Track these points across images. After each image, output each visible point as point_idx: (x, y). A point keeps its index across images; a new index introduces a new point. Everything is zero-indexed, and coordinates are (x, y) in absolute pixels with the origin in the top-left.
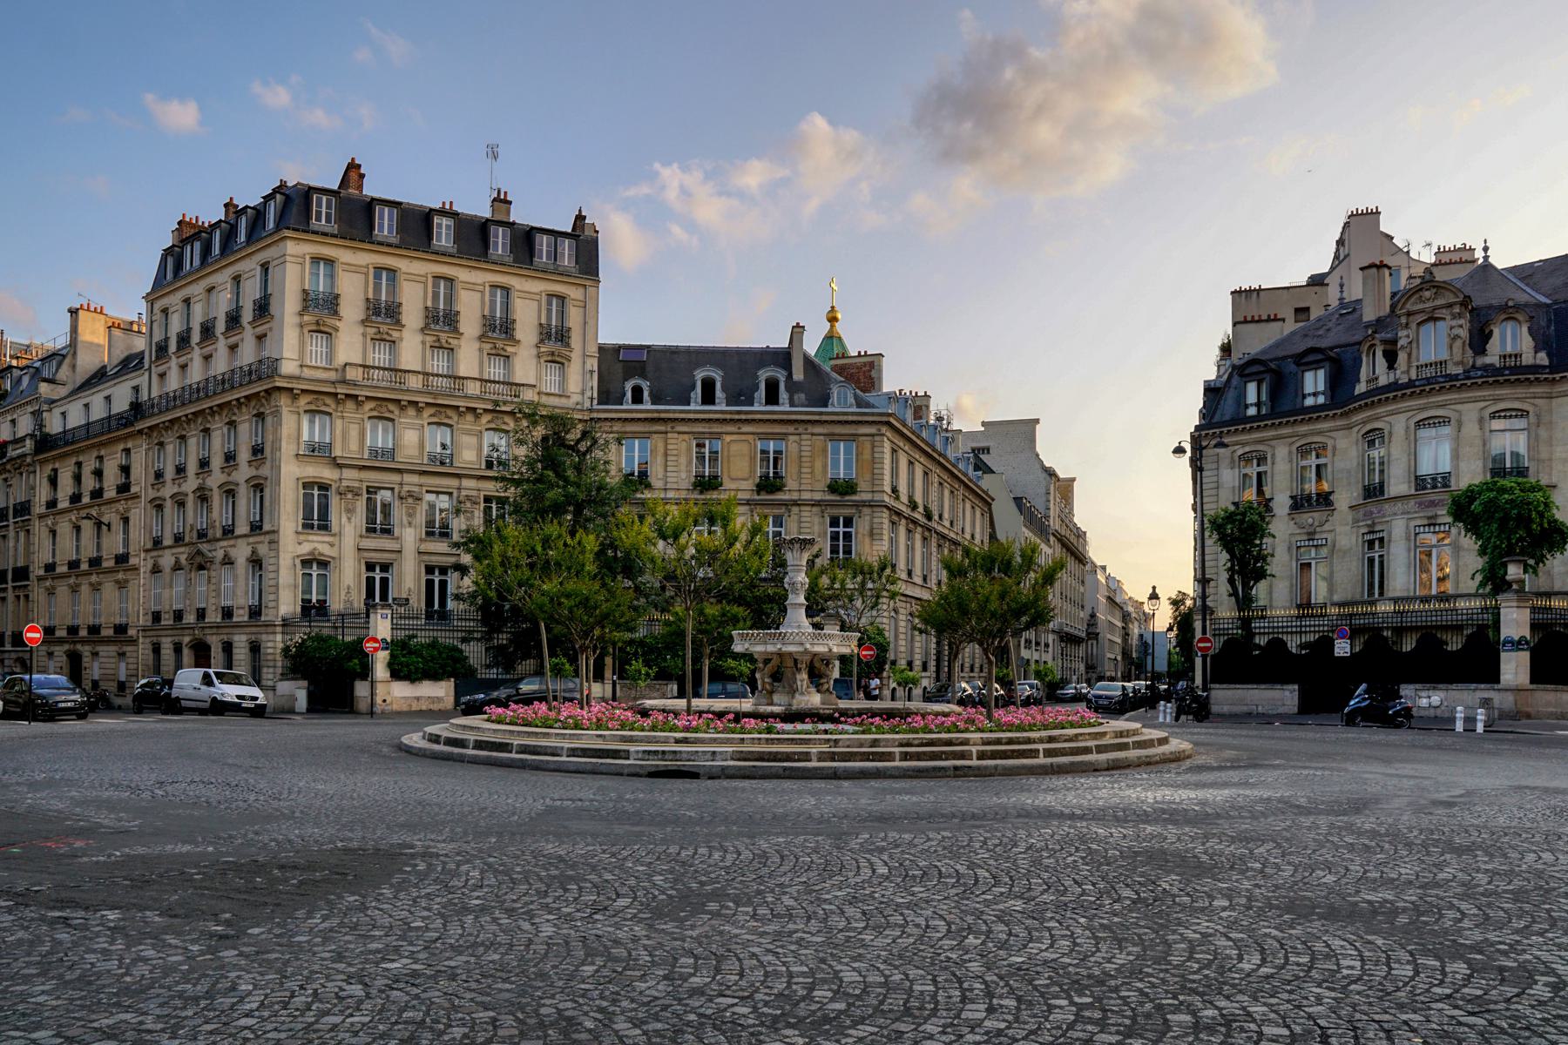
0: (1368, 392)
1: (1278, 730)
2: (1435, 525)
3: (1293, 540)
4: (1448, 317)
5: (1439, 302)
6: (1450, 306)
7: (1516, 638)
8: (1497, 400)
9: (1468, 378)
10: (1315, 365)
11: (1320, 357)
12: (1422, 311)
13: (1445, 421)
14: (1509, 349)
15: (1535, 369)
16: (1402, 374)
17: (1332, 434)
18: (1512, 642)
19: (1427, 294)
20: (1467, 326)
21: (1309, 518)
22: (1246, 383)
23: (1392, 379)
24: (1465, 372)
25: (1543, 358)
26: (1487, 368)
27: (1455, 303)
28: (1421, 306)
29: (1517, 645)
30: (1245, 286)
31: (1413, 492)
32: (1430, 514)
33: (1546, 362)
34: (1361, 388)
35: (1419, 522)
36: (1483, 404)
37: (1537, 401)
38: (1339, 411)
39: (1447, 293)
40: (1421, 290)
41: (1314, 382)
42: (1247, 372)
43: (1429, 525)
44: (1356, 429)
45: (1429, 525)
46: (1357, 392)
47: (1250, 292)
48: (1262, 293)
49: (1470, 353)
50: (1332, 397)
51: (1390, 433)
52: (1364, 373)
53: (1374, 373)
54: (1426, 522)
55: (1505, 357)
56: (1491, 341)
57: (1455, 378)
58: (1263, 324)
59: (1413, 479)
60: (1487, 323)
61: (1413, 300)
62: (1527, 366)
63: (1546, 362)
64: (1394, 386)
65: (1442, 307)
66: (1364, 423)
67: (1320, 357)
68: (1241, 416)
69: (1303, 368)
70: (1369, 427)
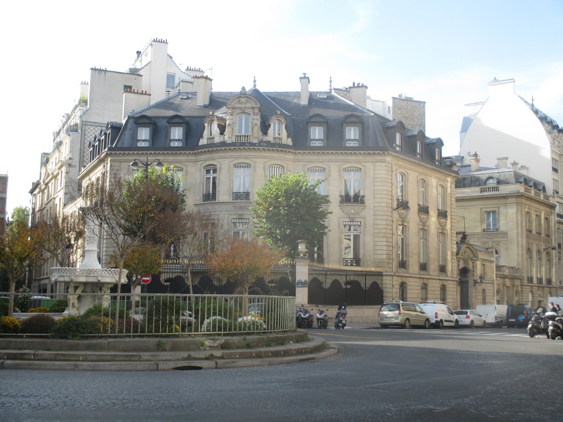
0: (207, 145)
1: (317, 329)
2: (242, 219)
3: (342, 220)
4: (252, 114)
5: (248, 105)
6: (253, 108)
7: (303, 281)
8: (347, 162)
9: (260, 146)
10: (177, 124)
11: (180, 121)
12: (240, 108)
13: (248, 166)
14: (243, 133)
15: (286, 146)
16: (228, 137)
17: (187, 164)
18: (301, 283)
19: (243, 100)
20: (260, 120)
21: (353, 208)
22: (138, 127)
23: (222, 140)
24: (259, 142)
25: (290, 142)
26: (268, 143)
27: (256, 107)
28: (239, 105)
29: (303, 284)
30: (98, 67)
31: (231, 200)
32: (240, 213)
33: (291, 144)
34: (203, 142)
35: (234, 217)
36: (265, 160)
37: (288, 162)
38: (191, 152)
39: (252, 101)
40: (240, 97)
41: (177, 133)
42: (172, 121)
43: (239, 219)
44: (200, 163)
45: (239, 219)
46: (200, 144)
47: (100, 70)
48: (107, 73)
49: (261, 133)
50: (186, 144)
51: (220, 169)
52: (206, 133)
53: (211, 134)
54: (237, 217)
55: (275, 138)
56: (270, 129)
57: (254, 145)
58: (140, 96)
59: (232, 194)
60: (268, 120)
61: (235, 101)
62: (284, 144)
63: (291, 144)
64: (223, 144)
65: (249, 108)
66: (205, 160)
67: (180, 121)
68: (134, 146)
69: (171, 125)
70: (208, 163)
